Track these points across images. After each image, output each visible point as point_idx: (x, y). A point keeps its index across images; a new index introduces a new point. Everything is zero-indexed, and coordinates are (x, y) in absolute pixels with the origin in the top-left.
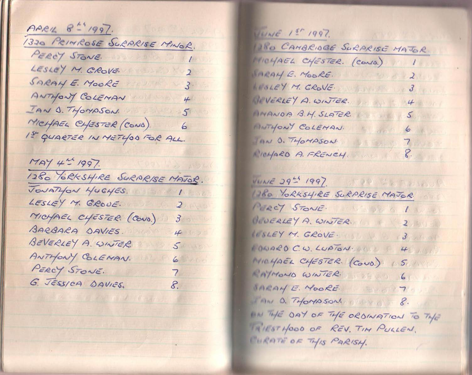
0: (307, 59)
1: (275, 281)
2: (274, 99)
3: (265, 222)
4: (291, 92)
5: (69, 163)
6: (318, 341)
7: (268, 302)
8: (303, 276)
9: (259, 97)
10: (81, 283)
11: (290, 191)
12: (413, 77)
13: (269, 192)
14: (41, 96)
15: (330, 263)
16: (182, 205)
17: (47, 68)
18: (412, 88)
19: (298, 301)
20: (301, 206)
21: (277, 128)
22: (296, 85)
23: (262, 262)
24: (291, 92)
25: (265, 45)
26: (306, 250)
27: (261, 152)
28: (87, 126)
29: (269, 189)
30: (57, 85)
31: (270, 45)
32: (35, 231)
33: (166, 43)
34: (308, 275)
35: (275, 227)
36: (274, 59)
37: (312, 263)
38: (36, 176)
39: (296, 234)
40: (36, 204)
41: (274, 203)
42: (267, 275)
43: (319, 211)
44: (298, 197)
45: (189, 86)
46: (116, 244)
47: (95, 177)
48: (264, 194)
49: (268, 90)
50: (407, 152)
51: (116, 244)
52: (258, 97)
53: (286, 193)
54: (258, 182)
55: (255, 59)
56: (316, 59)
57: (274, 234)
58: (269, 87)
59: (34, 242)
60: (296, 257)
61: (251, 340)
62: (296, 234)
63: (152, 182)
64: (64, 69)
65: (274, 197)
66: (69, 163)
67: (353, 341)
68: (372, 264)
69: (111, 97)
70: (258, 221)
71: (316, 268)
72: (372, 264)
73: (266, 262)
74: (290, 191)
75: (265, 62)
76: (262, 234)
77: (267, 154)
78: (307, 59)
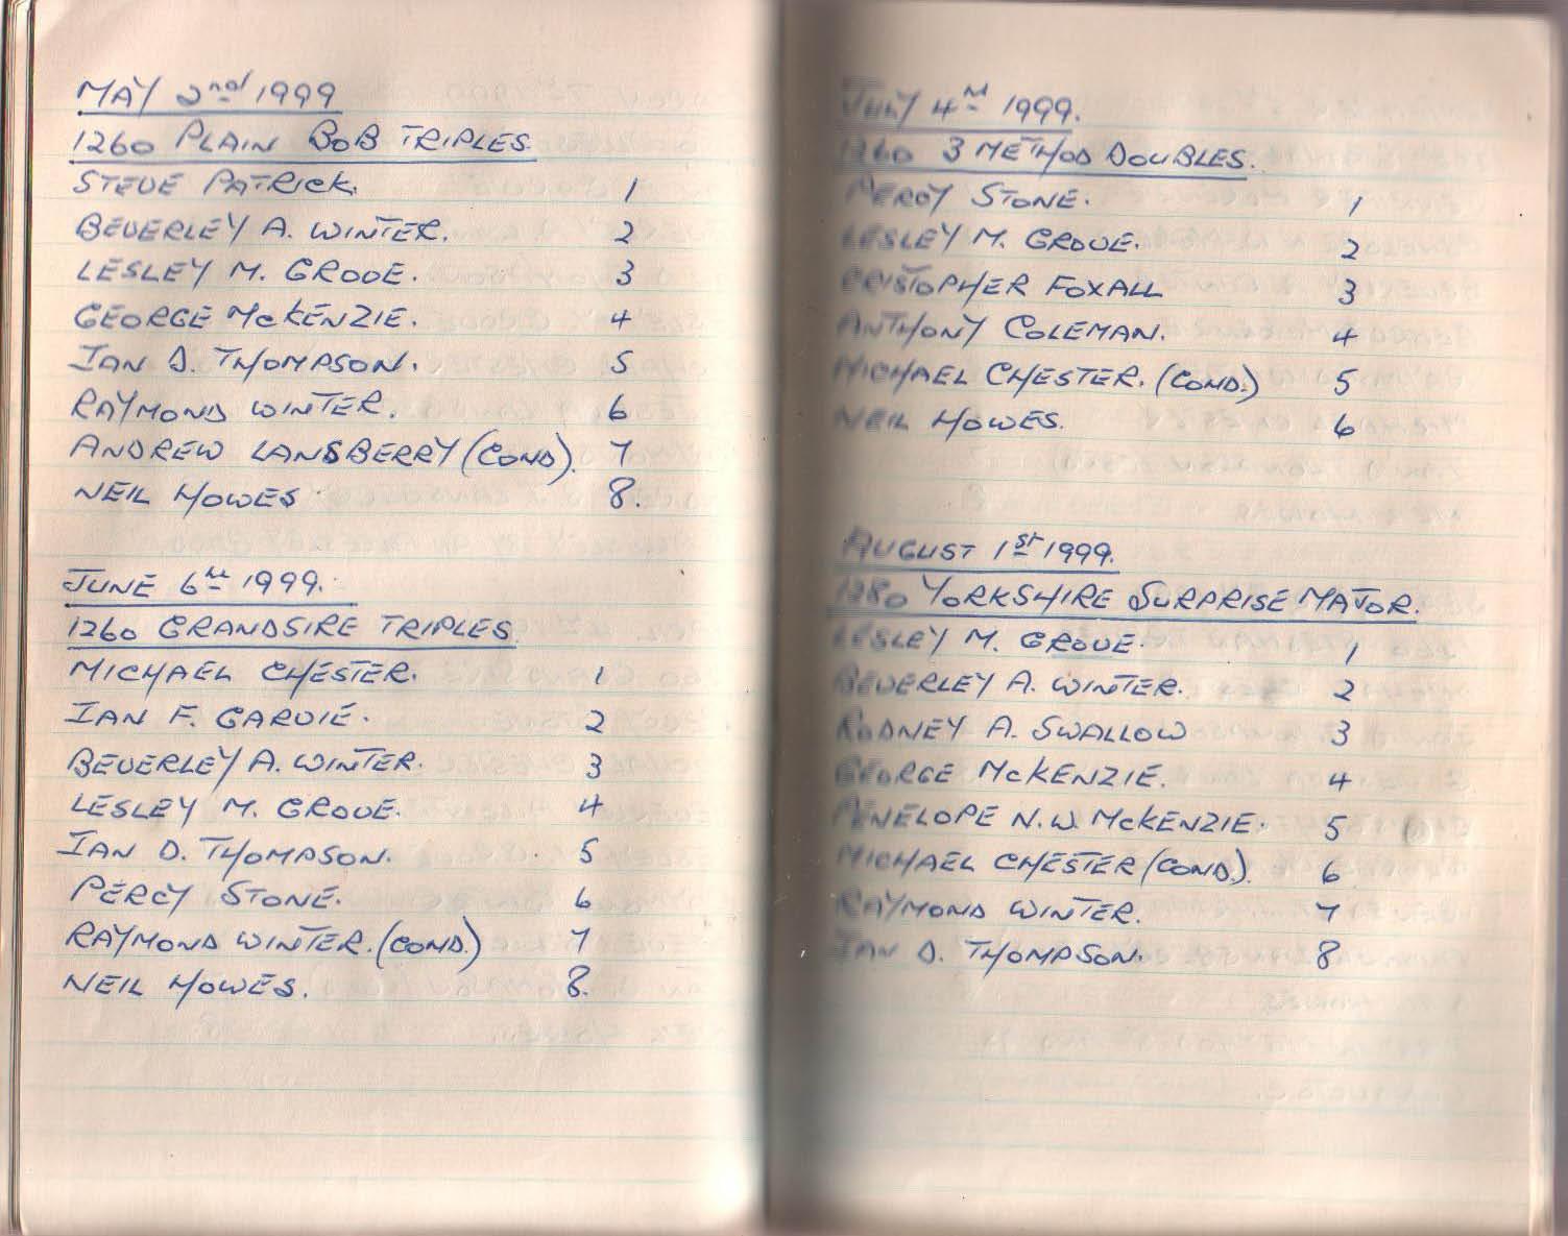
0: (1004, 367)
1: (922, 886)
2: (905, 812)
3: (878, 688)
4: (970, 787)
5: (213, 582)
6: (1117, 816)
7: (880, 952)
8: (1012, 912)
9: (857, 672)
10: (261, 716)
11: (961, 586)
12: (1354, 256)
13: (892, 589)
14: (129, 364)
15: (1097, 919)
16: (632, 236)
17: (896, 232)
18: (1350, 293)
19: (987, 954)
20: (1006, 189)
21: (919, 331)
22: (992, 232)
23: (869, 859)
24: (970, 787)
25: (873, 587)
26: (1001, 428)
27: (865, 898)
28: (1054, 155)
29: (892, 577)
30: (118, 721)
31: (899, 233)
32: (83, 769)
33: (1104, 815)
34: (1029, 910)
35: (916, 709)
36: (907, 856)
37: (1044, 869)
38: (95, 626)
39: (247, 806)
40: (165, 278)
41: (908, 628)
42: (117, 939)
43: (334, 416)
44: (994, 608)
45: (630, 273)
46: (366, 764)
47: (1061, 595)
48: (875, 594)
49: (886, 650)
50: (1325, 948)
51: (366, 764)
52: (852, 673)
53: (946, 593)
54: (868, 111)
55: (843, 415)
56: (987, 281)
57: (912, 639)
58: (889, 639)
59: (83, 762)
60: (983, 846)
61: (845, 283)
62: (247, 806)
63: (1248, 613)
64: (180, 493)
65: (915, 163)
66: (213, 582)
67: (1249, 598)
68: (1229, 384)
69: (293, 850)
70: (856, 686)
71: (1054, 890)
72: (1229, 384)
73: (906, 863)
74: (961, 586)
75: (877, 863)
76: (881, 236)
77: (893, 859)
78: (1004, 367)
